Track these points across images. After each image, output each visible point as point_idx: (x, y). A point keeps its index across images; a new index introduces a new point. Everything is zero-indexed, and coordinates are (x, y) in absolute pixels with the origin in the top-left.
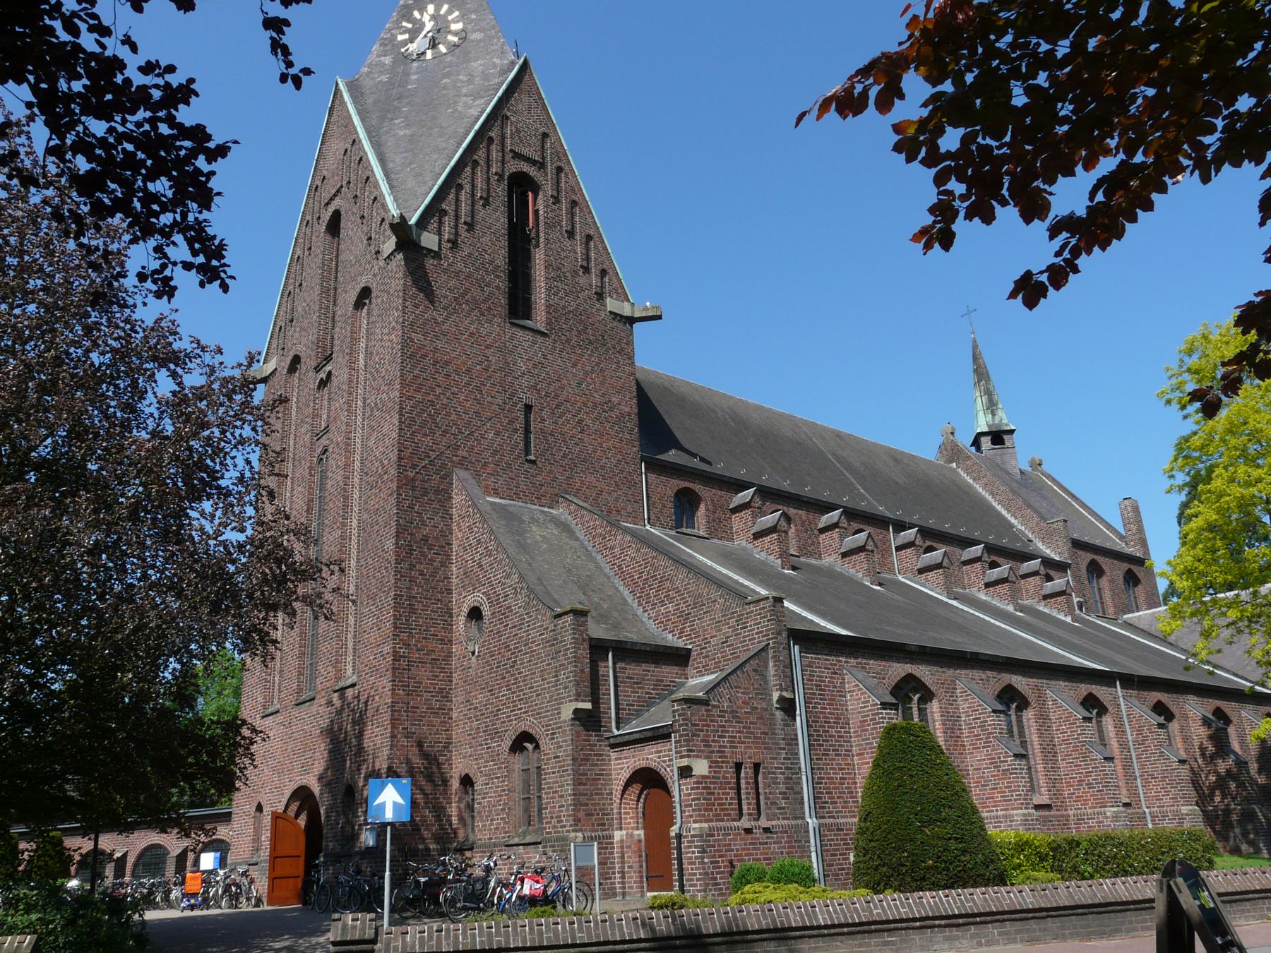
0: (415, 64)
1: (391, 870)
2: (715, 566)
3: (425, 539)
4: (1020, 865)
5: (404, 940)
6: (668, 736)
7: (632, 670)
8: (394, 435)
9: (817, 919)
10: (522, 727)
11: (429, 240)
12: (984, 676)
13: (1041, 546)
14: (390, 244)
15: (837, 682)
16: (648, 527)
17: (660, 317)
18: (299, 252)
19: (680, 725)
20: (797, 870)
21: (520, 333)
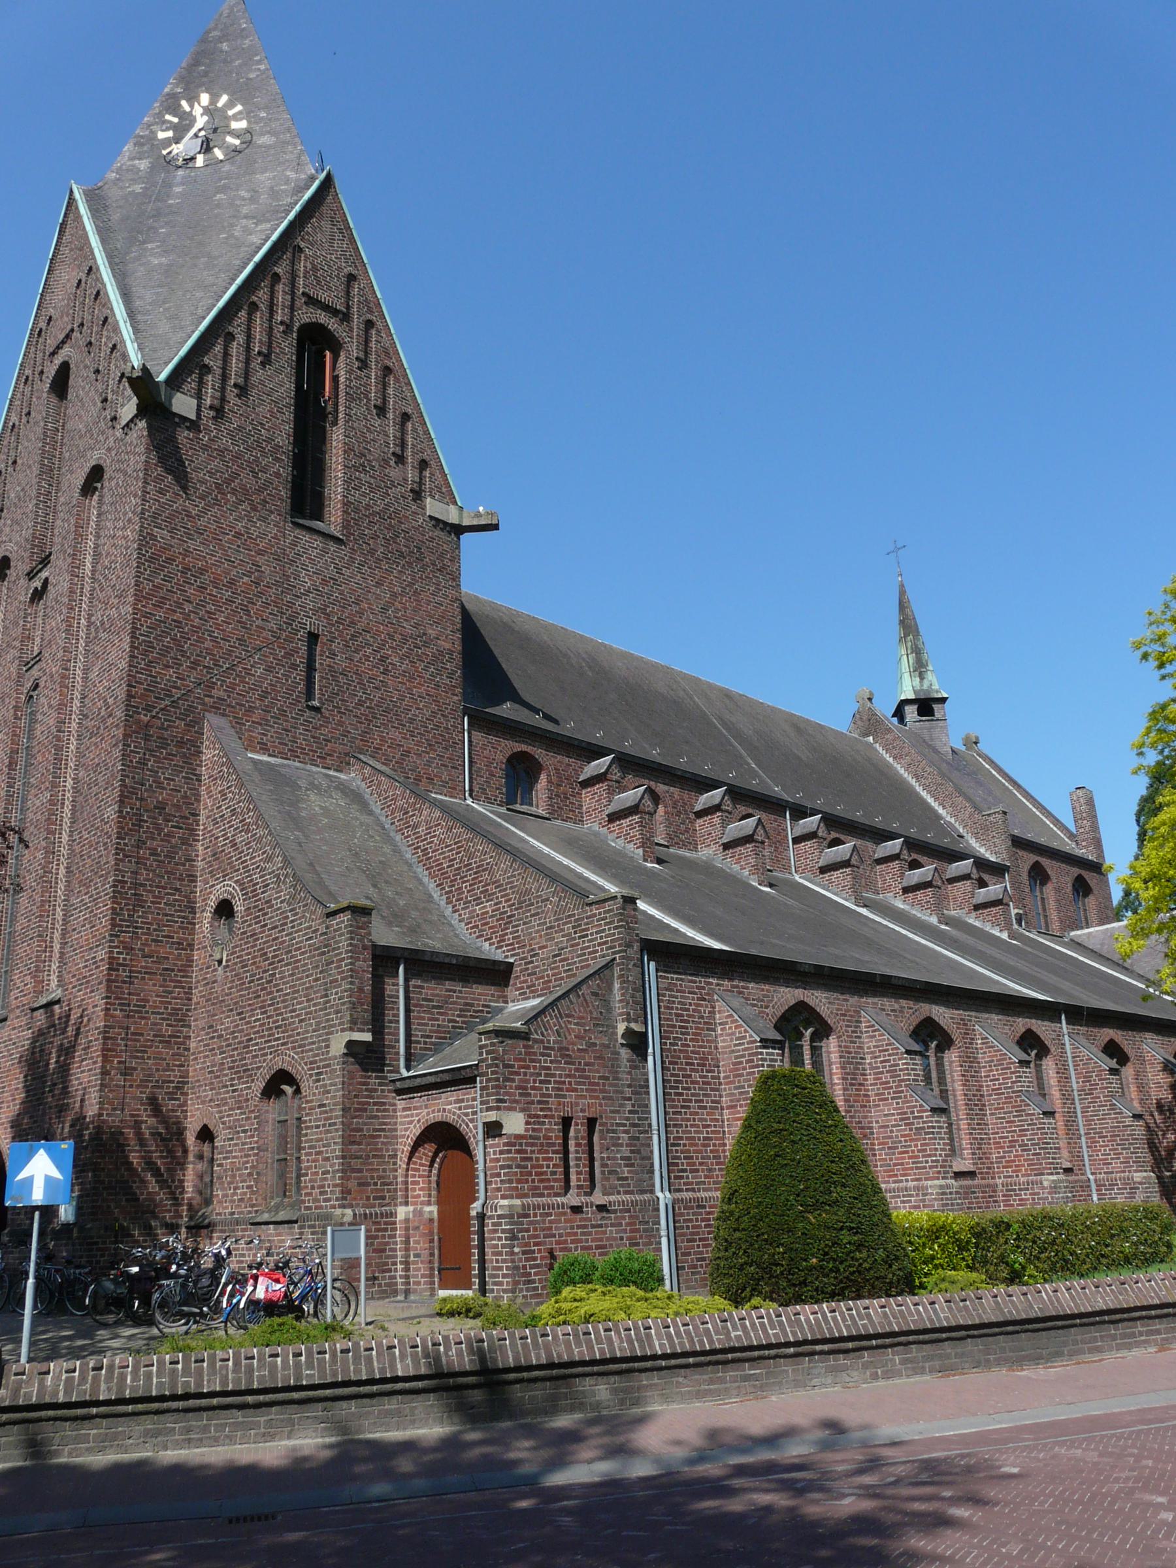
0: (180, 172)
1: (36, 1278)
2: (554, 854)
3: (161, 807)
4: (933, 1258)
5: (42, 1384)
6: (472, 1080)
7: (431, 989)
8: (123, 664)
9: (651, 1346)
10: (279, 1064)
11: (183, 404)
12: (896, 1006)
13: (973, 842)
14: (129, 408)
15: (706, 1010)
16: (469, 801)
17: (495, 527)
18: (14, 418)
19: (488, 1066)
20: (636, 1266)
21: (306, 537)
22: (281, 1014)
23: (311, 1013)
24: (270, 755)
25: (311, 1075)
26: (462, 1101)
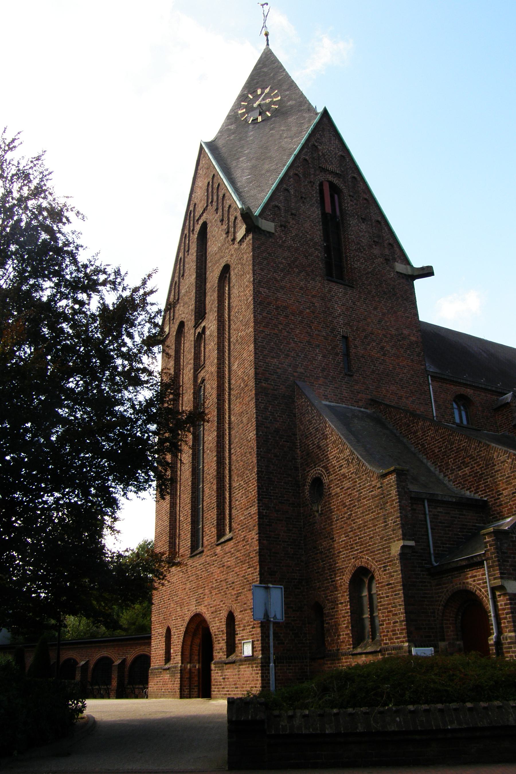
22: (358, 535)
23: (376, 533)
24: (329, 402)
25: (380, 568)
26: (475, 576)
